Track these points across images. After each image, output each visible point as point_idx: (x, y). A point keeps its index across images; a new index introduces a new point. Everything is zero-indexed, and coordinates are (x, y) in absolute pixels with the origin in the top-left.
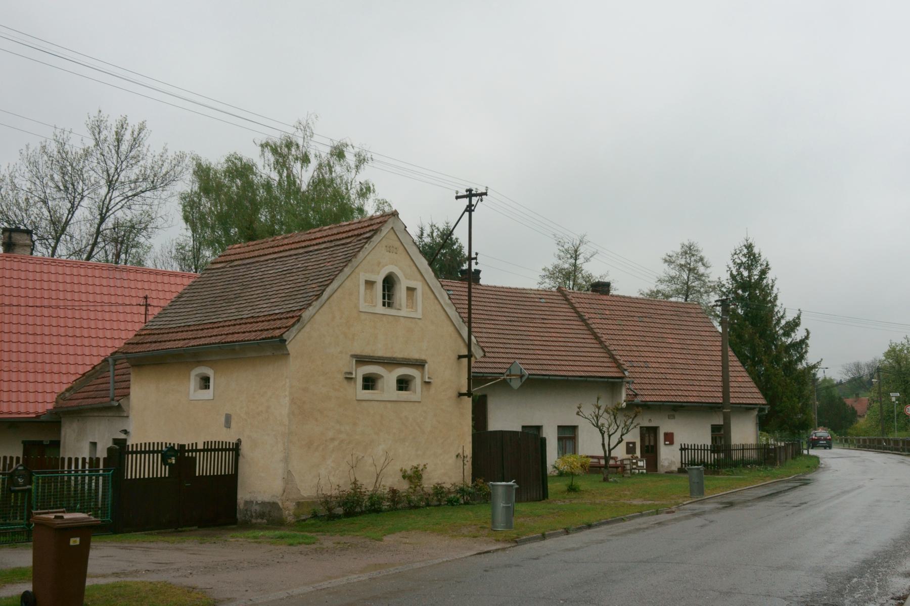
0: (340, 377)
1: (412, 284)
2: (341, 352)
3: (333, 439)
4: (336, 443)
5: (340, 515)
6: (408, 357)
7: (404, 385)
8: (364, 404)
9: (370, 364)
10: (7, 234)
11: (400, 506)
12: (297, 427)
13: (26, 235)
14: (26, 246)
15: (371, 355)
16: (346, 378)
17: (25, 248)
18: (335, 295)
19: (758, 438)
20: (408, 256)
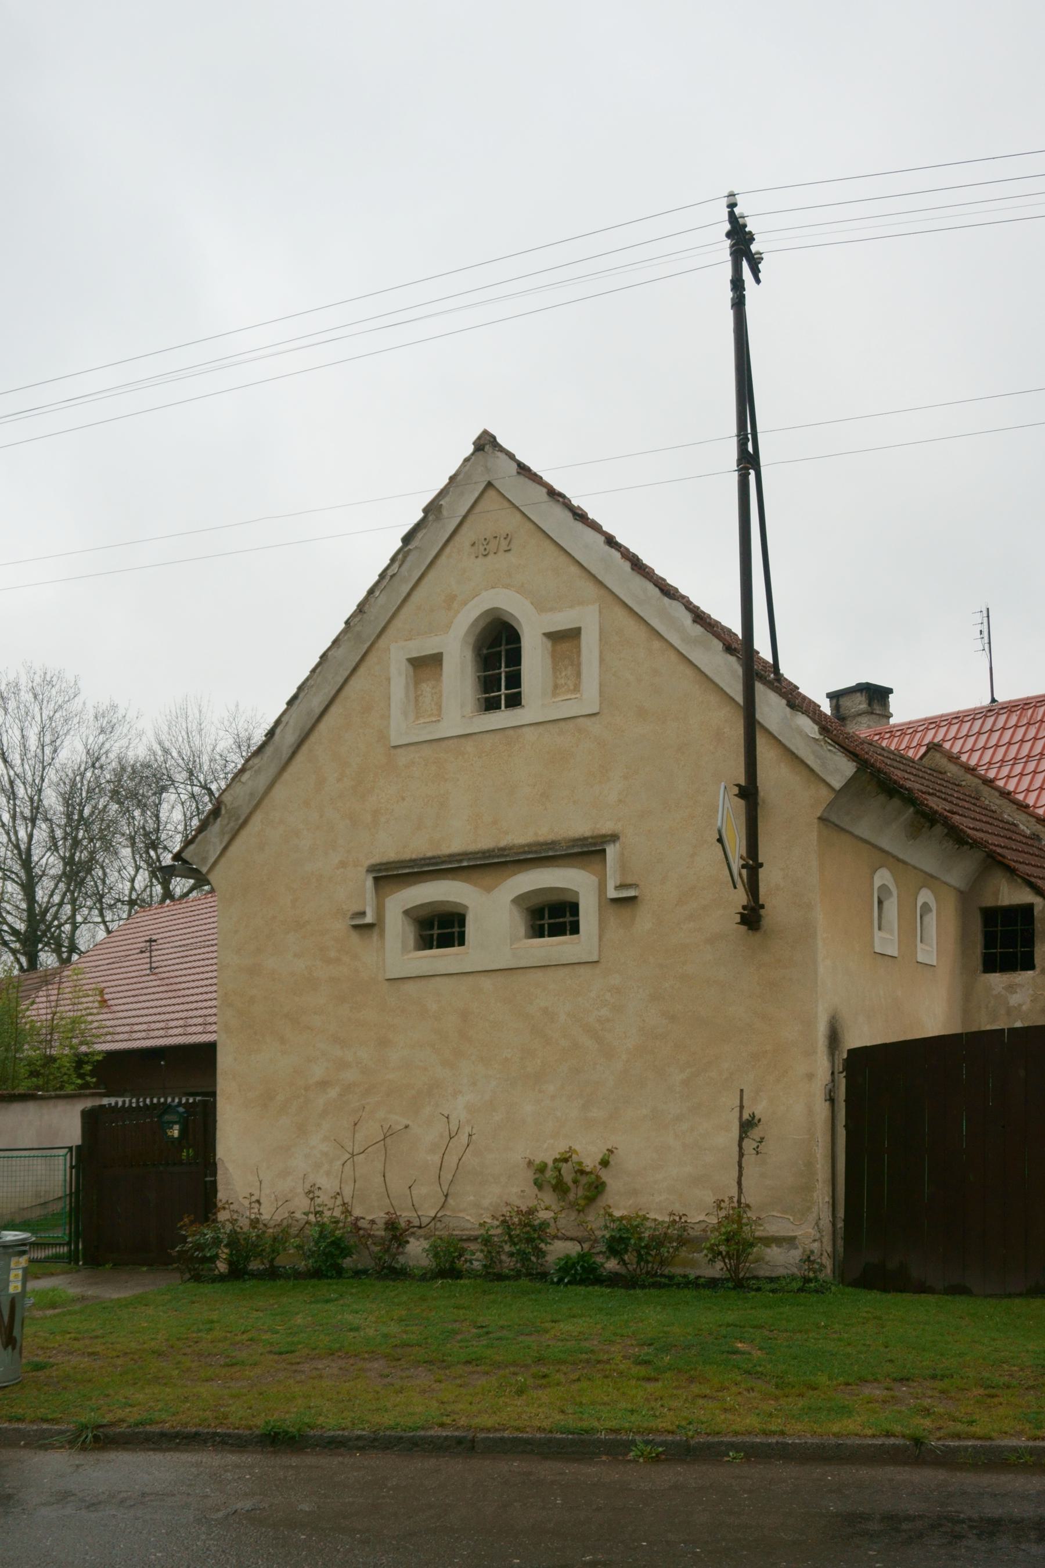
0: (340, 926)
1: (562, 621)
2: (343, 864)
3: (324, 1084)
4: (333, 1093)
5: (415, 1276)
6: (550, 837)
7: (568, 919)
8: (410, 987)
9: (415, 883)
10: (834, 701)
11: (347, 1263)
12: (235, 1059)
13: (859, 694)
14: (860, 715)
15: (429, 854)
16: (356, 927)
17: (859, 719)
18: (322, 726)
19: (967, 997)
20: (547, 543)
